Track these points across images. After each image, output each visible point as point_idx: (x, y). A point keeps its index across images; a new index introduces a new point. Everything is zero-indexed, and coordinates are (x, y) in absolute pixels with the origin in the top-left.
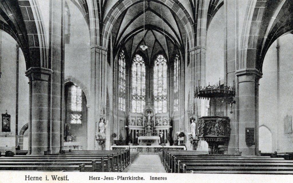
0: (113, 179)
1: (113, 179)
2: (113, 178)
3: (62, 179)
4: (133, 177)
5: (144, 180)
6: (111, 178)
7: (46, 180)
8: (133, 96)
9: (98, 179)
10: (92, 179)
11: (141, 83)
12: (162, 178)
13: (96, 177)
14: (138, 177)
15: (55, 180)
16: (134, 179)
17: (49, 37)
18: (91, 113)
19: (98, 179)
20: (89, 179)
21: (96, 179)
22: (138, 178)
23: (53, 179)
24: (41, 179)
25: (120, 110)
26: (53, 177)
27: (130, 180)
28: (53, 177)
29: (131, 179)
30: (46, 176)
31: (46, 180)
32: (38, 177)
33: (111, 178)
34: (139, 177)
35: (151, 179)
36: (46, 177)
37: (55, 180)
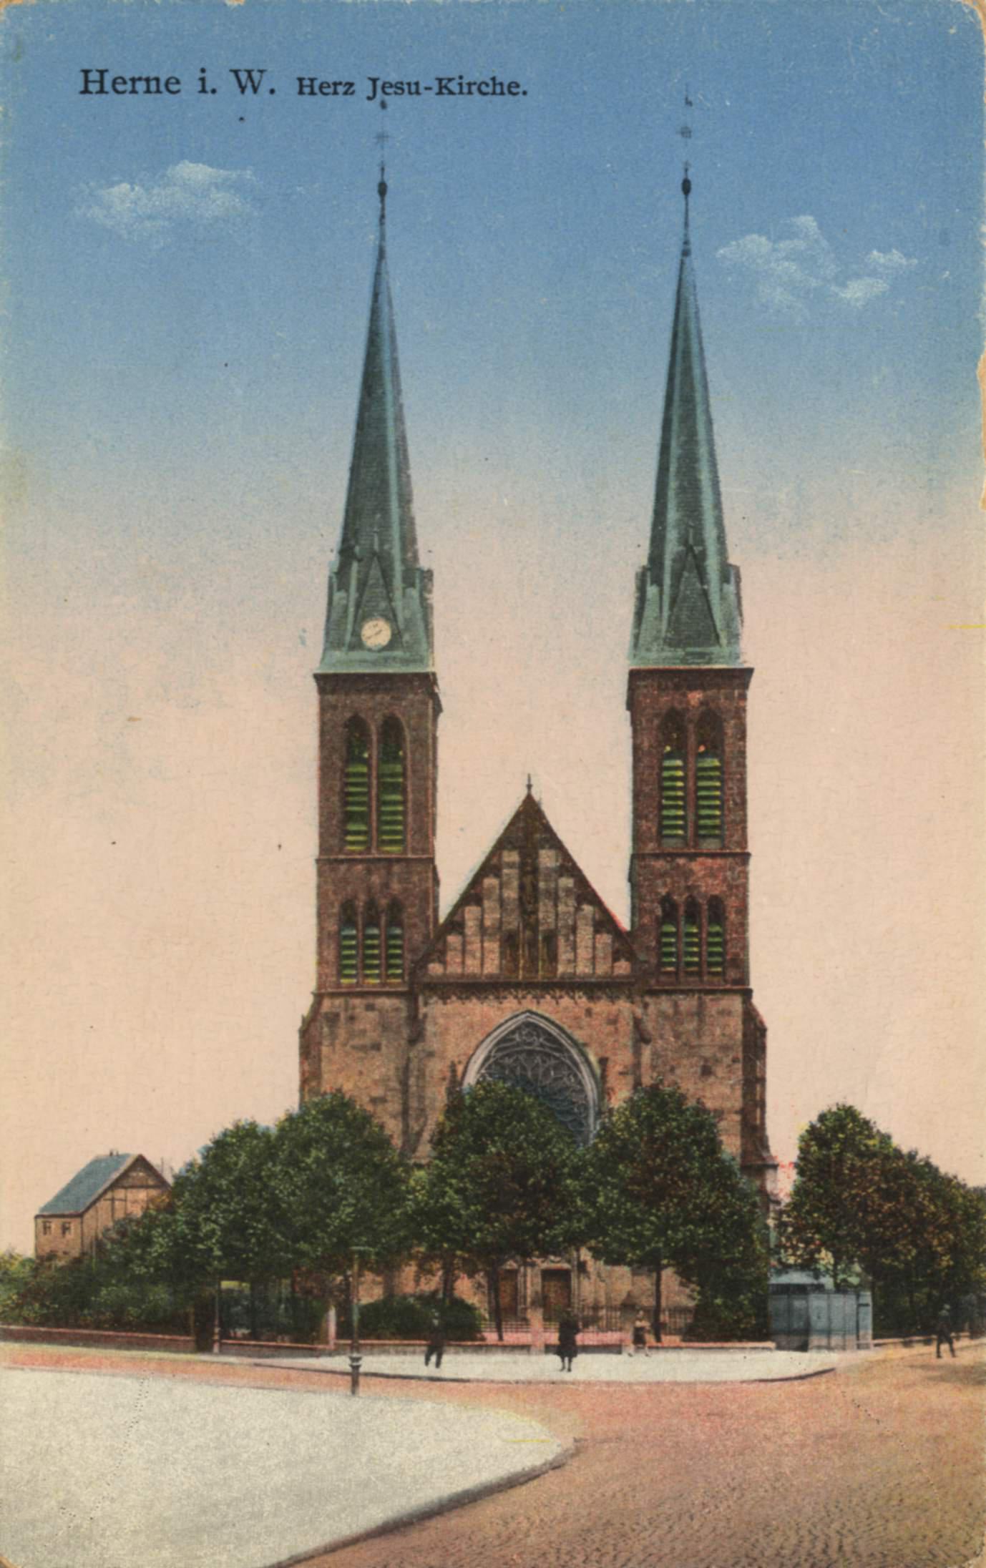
0: (418, 93)
1: (418, 93)
2: (417, 84)
3: (400, 91)
4: (465, 81)
5: (525, 93)
6: (406, 87)
7: (203, 91)
8: (641, 1119)
9: (341, 89)
10: (312, 93)
11: (356, 1368)
12: (474, 88)
13: (127, 76)
14: (493, 79)
15: (255, 90)
16: (470, 93)
17: (45, 1373)
18: (931, 511)
19: (341, 89)
20: (297, 89)
21: (129, 87)
22: (494, 85)
23: (243, 89)
24: (174, 87)
25: (907, 1263)
26: (243, 76)
27: (446, 97)
28: (243, 76)
29: (451, 93)
30: (203, 71)
31: (203, 91)
32: (157, 80)
33: (406, 87)
34: (498, 81)
35: (86, 91)
36: (203, 80)
37: (255, 90)
